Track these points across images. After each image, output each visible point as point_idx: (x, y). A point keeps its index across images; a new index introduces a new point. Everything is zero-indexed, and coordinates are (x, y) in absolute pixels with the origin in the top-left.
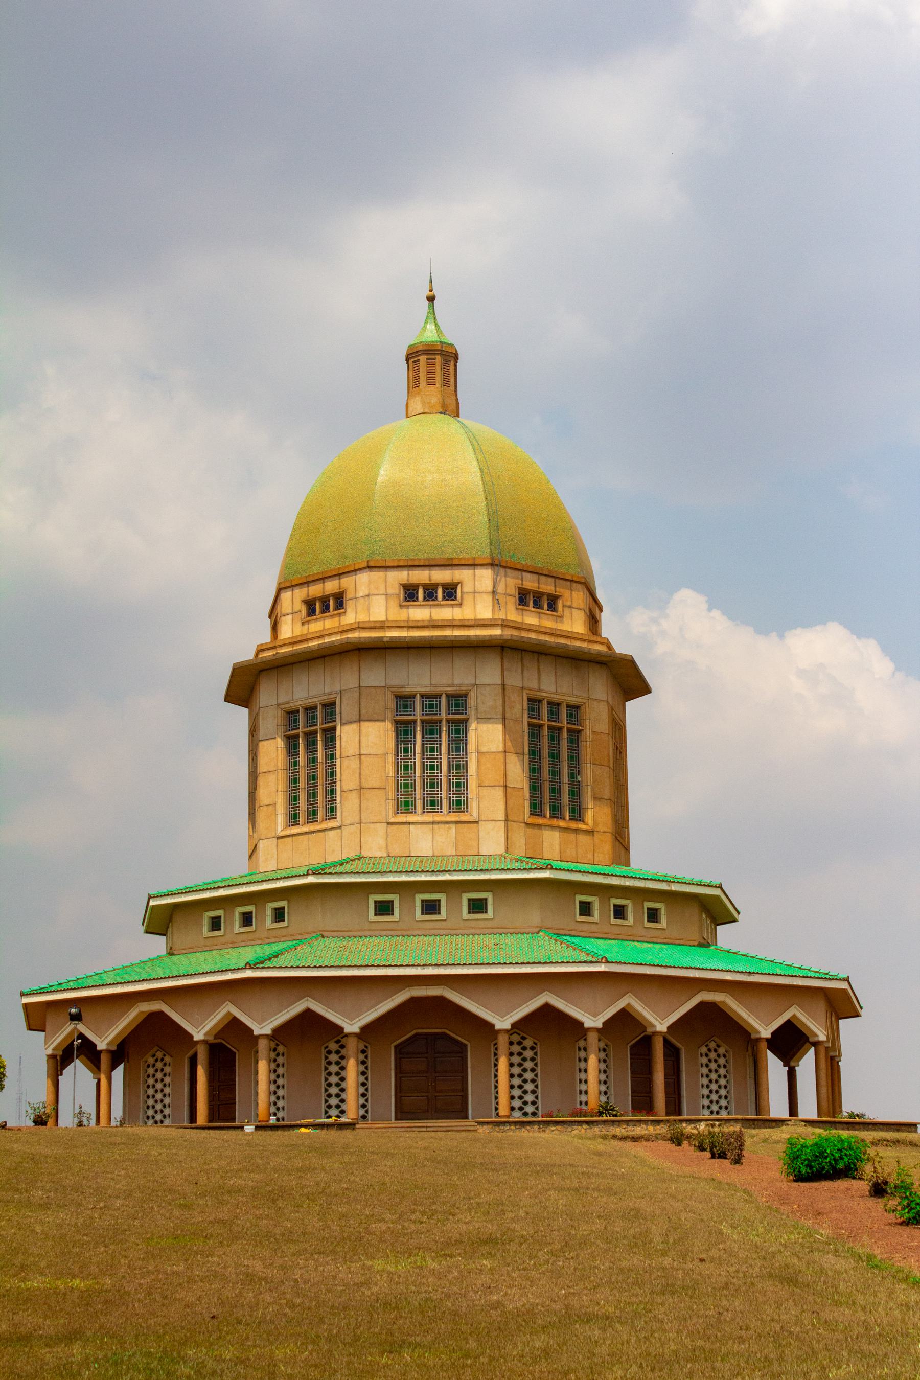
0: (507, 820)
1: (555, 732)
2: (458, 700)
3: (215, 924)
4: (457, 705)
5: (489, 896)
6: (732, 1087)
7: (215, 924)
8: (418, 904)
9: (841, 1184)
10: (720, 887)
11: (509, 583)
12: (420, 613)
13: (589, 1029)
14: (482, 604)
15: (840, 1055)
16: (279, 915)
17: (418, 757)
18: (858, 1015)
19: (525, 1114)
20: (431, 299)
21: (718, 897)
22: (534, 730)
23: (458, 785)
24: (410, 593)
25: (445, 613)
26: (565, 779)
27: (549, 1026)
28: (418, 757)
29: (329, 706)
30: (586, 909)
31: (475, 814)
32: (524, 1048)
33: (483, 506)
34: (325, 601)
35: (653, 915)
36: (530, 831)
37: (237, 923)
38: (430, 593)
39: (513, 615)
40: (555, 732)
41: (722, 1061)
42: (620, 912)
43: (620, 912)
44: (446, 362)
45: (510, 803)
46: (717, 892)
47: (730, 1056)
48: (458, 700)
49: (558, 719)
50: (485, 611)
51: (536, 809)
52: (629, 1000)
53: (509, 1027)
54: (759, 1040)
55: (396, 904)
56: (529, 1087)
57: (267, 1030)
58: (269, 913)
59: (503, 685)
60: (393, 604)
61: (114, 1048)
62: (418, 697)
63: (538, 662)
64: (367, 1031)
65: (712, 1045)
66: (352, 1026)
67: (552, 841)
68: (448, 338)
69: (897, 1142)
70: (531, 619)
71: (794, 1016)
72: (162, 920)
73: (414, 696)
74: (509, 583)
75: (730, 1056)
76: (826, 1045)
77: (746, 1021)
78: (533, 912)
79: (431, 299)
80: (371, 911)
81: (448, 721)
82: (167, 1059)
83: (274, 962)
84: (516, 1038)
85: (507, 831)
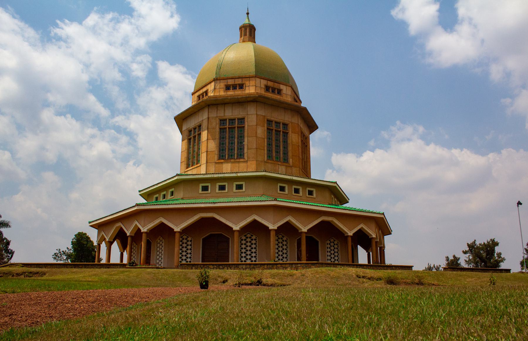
0: (207, 162)
2: (285, 125)
3: (164, 196)
4: (241, 122)
5: (209, 185)
6: (288, 253)
8: (235, 186)
10: (336, 183)
11: (222, 84)
12: (231, 93)
13: (271, 230)
14: (251, 89)
15: (384, 247)
17: (227, 140)
18: (391, 234)
19: (187, 262)
20: (248, 14)
21: (335, 187)
22: (222, 130)
23: (241, 149)
24: (228, 88)
25: (238, 93)
26: (282, 148)
27: (255, 228)
28: (227, 140)
29: (200, 126)
30: (282, 189)
32: (252, 240)
33: (254, 59)
35: (310, 193)
36: (217, 165)
37: (161, 198)
38: (234, 87)
40: (232, 129)
42: (297, 191)
43: (297, 191)
45: (209, 157)
46: (335, 185)
47: (339, 244)
48: (242, 120)
51: (270, 157)
52: (290, 218)
53: (276, 228)
54: (348, 236)
55: (227, 186)
57: (276, 228)
58: (162, 196)
59: (208, 118)
61: (133, 235)
62: (274, 122)
63: (224, 110)
64: (185, 231)
65: (332, 240)
68: (252, 23)
71: (362, 227)
72: (148, 195)
73: (280, 123)
74: (264, 82)
76: (376, 240)
77: (342, 229)
79: (248, 14)
80: (279, 189)
81: (238, 127)
82: (163, 240)
85: (206, 167)
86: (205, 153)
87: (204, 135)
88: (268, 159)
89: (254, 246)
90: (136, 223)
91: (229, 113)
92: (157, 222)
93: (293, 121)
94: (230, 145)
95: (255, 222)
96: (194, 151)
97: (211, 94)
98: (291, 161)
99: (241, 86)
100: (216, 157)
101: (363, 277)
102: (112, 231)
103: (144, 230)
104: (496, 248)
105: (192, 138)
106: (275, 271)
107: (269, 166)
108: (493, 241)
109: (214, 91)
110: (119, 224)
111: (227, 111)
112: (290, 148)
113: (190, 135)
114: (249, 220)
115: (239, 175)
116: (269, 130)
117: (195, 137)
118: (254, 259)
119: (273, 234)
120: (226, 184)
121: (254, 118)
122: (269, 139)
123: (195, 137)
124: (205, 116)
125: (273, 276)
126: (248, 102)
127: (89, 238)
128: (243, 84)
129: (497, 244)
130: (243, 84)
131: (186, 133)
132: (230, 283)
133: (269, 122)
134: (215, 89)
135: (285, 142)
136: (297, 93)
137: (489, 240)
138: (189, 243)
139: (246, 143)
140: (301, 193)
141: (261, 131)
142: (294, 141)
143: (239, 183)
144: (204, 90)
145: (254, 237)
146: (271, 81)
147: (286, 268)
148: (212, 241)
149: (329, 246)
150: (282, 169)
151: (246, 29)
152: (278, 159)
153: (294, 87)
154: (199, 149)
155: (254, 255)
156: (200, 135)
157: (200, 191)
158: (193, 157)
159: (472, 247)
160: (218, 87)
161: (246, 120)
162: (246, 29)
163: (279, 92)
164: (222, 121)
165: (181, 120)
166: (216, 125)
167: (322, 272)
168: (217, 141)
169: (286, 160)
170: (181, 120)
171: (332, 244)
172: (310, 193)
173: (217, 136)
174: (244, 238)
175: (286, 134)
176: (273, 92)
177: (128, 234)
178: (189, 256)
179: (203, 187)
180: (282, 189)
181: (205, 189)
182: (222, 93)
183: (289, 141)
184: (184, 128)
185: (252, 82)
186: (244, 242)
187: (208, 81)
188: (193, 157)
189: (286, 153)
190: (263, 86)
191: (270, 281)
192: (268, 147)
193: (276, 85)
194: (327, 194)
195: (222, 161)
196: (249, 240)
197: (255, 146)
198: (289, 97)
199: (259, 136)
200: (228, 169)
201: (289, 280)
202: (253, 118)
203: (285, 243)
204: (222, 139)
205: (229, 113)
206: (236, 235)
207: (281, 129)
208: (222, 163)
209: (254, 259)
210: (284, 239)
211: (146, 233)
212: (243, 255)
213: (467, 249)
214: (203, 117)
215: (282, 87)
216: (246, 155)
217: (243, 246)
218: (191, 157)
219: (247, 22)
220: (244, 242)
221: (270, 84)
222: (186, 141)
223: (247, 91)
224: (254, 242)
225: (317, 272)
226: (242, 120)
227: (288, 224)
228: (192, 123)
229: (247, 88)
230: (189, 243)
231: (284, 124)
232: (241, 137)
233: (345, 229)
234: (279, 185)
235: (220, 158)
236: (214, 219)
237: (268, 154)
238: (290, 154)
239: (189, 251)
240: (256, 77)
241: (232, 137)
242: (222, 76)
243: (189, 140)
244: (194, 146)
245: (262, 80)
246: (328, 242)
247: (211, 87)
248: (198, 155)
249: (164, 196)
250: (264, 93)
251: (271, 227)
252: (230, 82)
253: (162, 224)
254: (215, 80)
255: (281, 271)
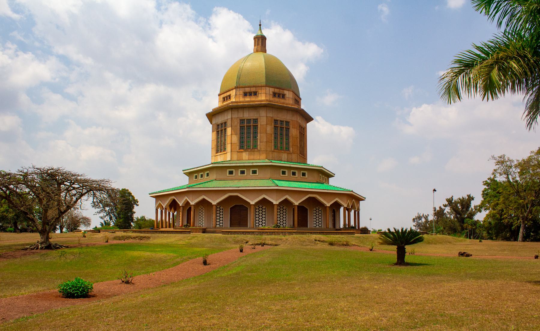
0: (231, 151)
1: (282, 128)
2: (287, 123)
3: (202, 176)
5: (234, 170)
6: (287, 218)
7: (196, 177)
8: (239, 172)
9: (419, 244)
11: (241, 92)
12: (248, 99)
14: (263, 97)
16: (208, 175)
20: (260, 25)
22: (242, 128)
24: (245, 94)
25: (253, 98)
27: (264, 202)
29: (225, 123)
30: (284, 173)
31: (259, 148)
33: (264, 74)
34: (227, 97)
36: (239, 154)
38: (250, 94)
39: (272, 99)
40: (249, 127)
41: (320, 212)
42: (294, 174)
44: (262, 40)
46: (352, 193)
48: (256, 120)
49: (278, 124)
50: (263, 98)
51: (241, 147)
52: (204, 197)
54: (327, 207)
56: (264, 219)
57: (278, 203)
58: (200, 176)
59: (232, 118)
60: (271, 96)
64: (257, 203)
65: (317, 208)
66: (214, 203)
67: (245, 155)
69: (243, 233)
70: (277, 99)
74: (272, 90)
75: (287, 209)
78: (268, 173)
79: (260, 25)
80: (251, 173)
83: (198, 186)
84: (218, 207)
86: (230, 145)
87: (229, 130)
88: (274, 149)
89: (264, 216)
90: (186, 198)
91: (247, 115)
92: (201, 198)
93: (293, 119)
94: (248, 136)
95: (264, 199)
96: (221, 141)
97: (233, 100)
98: (291, 149)
99: (255, 94)
100: (238, 148)
101: (319, 241)
102: (168, 201)
103: (192, 203)
104: (472, 202)
105: (220, 131)
106: (273, 236)
107: (275, 154)
108: (469, 196)
109: (235, 98)
110: (173, 197)
111: (245, 114)
112: (291, 140)
113: (218, 128)
114: (261, 198)
115: (254, 164)
116: (276, 127)
117: (222, 130)
118: (264, 224)
119: (275, 207)
120: (245, 170)
121: (265, 118)
122: (276, 134)
123: (222, 130)
124: (229, 116)
125: (272, 240)
126: (262, 106)
127: (131, 194)
128: (256, 92)
129: (473, 199)
130: (256, 92)
131: (216, 127)
132: (250, 243)
133: (276, 121)
134: (236, 95)
135: (287, 135)
136: (297, 94)
137: (440, 202)
138: (221, 211)
139: (259, 137)
140: (297, 175)
141: (270, 129)
142: (294, 134)
143: (255, 169)
144: (228, 94)
145: (264, 207)
146: (277, 88)
147: (279, 234)
148: (237, 210)
149: (315, 212)
150: (284, 156)
151: (259, 40)
152: (282, 149)
153: (296, 92)
154: (225, 140)
155: (264, 219)
156: (225, 129)
157: (228, 174)
158: (221, 146)
159: (450, 201)
160: (238, 94)
161: (259, 120)
162: (259, 40)
163: (284, 96)
164: (242, 121)
165: (211, 116)
166: (237, 123)
167: (297, 238)
168: (238, 135)
169: (288, 149)
170: (211, 116)
171: (317, 211)
172: (304, 174)
173: (238, 132)
174: (257, 208)
175: (288, 129)
176: (279, 96)
177: (181, 205)
178: (221, 222)
179: (229, 171)
180: (284, 173)
181: (231, 173)
182: (242, 99)
183: (290, 135)
184: (214, 122)
185: (263, 91)
186: (257, 210)
187: (231, 88)
188: (221, 146)
189: (288, 143)
190: (271, 93)
191: (270, 242)
192: (274, 140)
193: (281, 92)
194: (315, 174)
195: (242, 150)
196: (261, 209)
197: (265, 140)
198: (291, 99)
199: (268, 132)
200: (246, 159)
201: (279, 242)
202: (264, 119)
203: (284, 211)
204: (242, 134)
205: (247, 115)
206: (252, 207)
207: (284, 126)
208: (242, 152)
209: (264, 224)
210: (284, 208)
211: (194, 205)
212: (257, 219)
213: (447, 203)
214: (227, 117)
215: (286, 92)
216: (259, 146)
217: (257, 213)
218: (220, 147)
219: (260, 34)
220: (257, 210)
221: (277, 91)
222: (215, 133)
223: (259, 99)
224: (264, 210)
225: (294, 238)
226: (256, 120)
227: (286, 200)
228: (219, 120)
229: (260, 95)
230: (221, 211)
231: (286, 122)
232: (255, 133)
233: (325, 202)
234: (282, 170)
235: (240, 149)
236: (237, 196)
237: (274, 145)
238: (291, 144)
239: (221, 216)
240: (266, 86)
241: (249, 133)
242: (241, 85)
243: (218, 132)
244: (221, 137)
245: (271, 89)
246: (315, 209)
247: (233, 93)
248: (225, 144)
249: (202, 176)
250: (272, 99)
251: (275, 203)
252: (247, 90)
253: (204, 199)
254: (236, 88)
255: (276, 237)
